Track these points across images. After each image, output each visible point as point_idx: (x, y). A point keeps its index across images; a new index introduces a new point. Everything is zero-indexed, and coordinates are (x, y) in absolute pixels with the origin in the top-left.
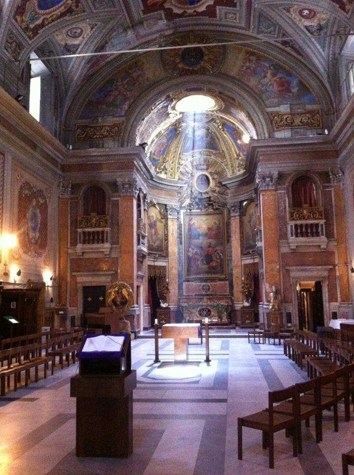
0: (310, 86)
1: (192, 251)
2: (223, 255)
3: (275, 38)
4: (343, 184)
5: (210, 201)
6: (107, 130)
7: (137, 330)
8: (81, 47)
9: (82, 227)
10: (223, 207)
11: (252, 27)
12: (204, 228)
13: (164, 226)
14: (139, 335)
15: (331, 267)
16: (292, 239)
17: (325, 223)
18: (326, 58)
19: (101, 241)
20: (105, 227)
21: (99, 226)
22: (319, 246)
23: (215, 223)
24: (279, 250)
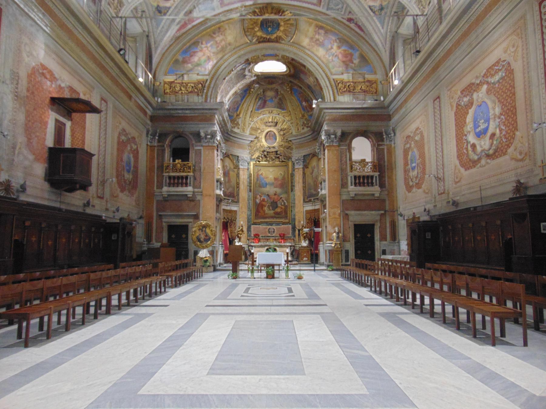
3: (342, 15)
5: (277, 154)
8: (171, 10)
10: (288, 160)
11: (322, 4)
15: (383, 212)
17: (379, 175)
19: (184, 185)
20: (189, 172)
21: (183, 172)
22: (373, 195)
23: (281, 174)
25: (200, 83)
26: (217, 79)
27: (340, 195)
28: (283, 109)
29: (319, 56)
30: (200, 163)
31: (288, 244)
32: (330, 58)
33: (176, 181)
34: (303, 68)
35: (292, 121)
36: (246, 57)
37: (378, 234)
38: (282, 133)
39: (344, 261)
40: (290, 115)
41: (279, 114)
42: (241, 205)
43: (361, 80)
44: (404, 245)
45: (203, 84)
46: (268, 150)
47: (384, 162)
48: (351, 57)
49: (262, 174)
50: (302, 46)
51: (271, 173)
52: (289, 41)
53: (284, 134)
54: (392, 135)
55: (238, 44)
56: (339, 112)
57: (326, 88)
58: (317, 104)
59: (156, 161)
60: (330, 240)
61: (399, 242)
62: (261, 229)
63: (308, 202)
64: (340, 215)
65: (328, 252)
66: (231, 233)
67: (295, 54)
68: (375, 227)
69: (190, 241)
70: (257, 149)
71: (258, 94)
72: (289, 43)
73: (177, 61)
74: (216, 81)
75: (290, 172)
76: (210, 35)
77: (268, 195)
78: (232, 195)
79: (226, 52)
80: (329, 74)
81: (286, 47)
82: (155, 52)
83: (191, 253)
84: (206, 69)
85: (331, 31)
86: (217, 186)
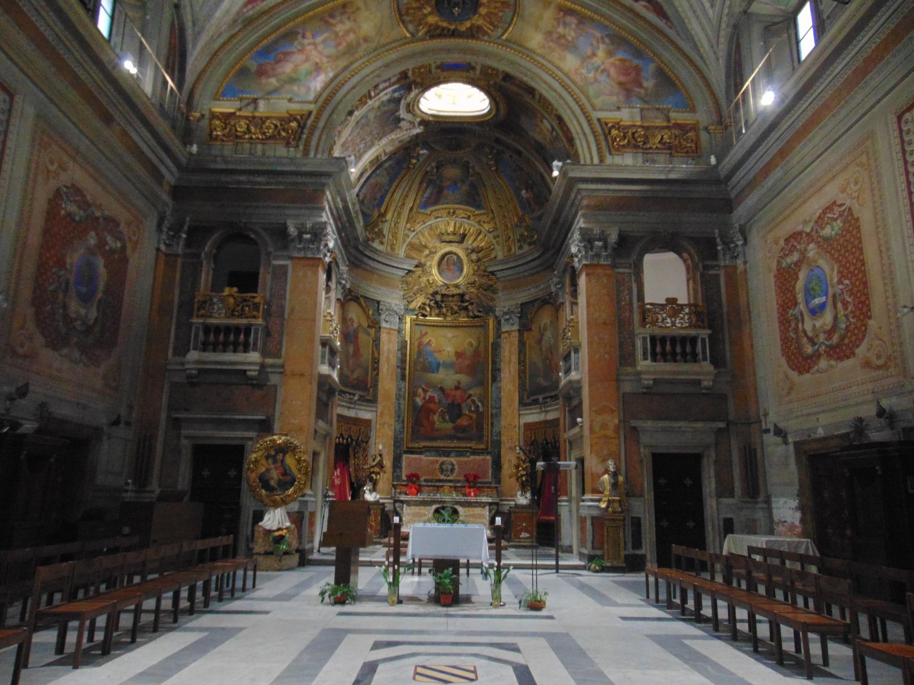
0: (678, 78)
1: (422, 395)
2: (483, 405)
4: (745, 262)
5: (462, 301)
6: (276, 126)
7: (307, 547)
9: (202, 316)
10: (487, 313)
12: (449, 352)
13: (374, 341)
14: (310, 557)
16: (644, 364)
17: (710, 336)
18: (714, 23)
19: (241, 348)
20: (254, 317)
21: (241, 316)
22: (698, 382)
24: (618, 389)
25: (295, 119)
26: (333, 112)
27: (617, 380)
28: (478, 207)
29: (566, 70)
30: (283, 297)
31: (484, 499)
32: (591, 75)
33: (221, 338)
34: (527, 98)
35: (496, 233)
36: (402, 68)
37: (713, 480)
38: (474, 257)
39: (630, 545)
40: (494, 218)
41: (469, 218)
42: (380, 408)
43: (660, 122)
44: (787, 509)
45: (302, 119)
46: (444, 292)
47: (720, 304)
48: (638, 74)
49: (429, 343)
50: (528, 49)
51: (447, 342)
52: (500, 37)
53: (479, 260)
54: (740, 243)
55: (383, 41)
56: (614, 190)
57: (581, 136)
58: (561, 170)
59: (177, 292)
60: (595, 491)
61: (768, 501)
62: (421, 462)
63: (530, 404)
64: (617, 429)
65: (589, 522)
66: (355, 470)
67: (512, 63)
68: (705, 461)
69: (244, 486)
70: (421, 290)
71: (427, 173)
72: (499, 41)
73: (243, 72)
74: (331, 115)
75: (491, 340)
76: (322, 19)
77: (442, 389)
78: (362, 386)
79: (357, 56)
80: (588, 107)
81: (492, 48)
82: (194, 45)
83: (247, 516)
84: (309, 89)
85: (592, 20)
86: (323, 357)
